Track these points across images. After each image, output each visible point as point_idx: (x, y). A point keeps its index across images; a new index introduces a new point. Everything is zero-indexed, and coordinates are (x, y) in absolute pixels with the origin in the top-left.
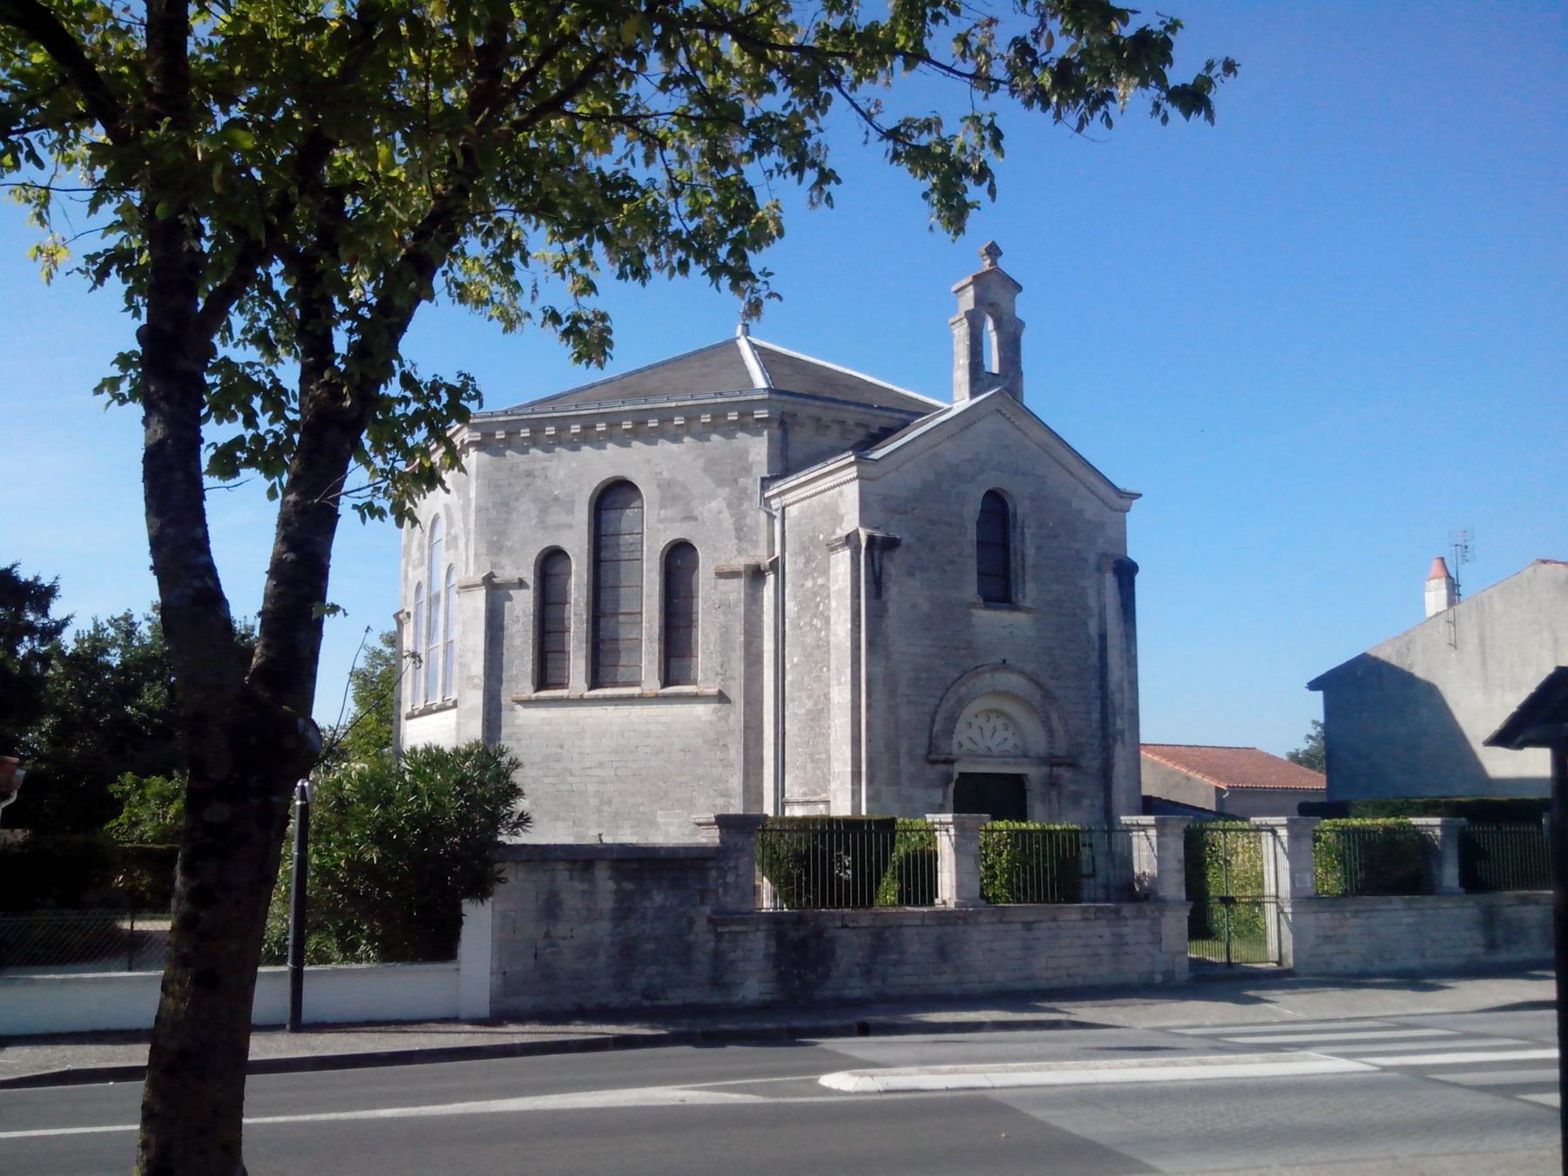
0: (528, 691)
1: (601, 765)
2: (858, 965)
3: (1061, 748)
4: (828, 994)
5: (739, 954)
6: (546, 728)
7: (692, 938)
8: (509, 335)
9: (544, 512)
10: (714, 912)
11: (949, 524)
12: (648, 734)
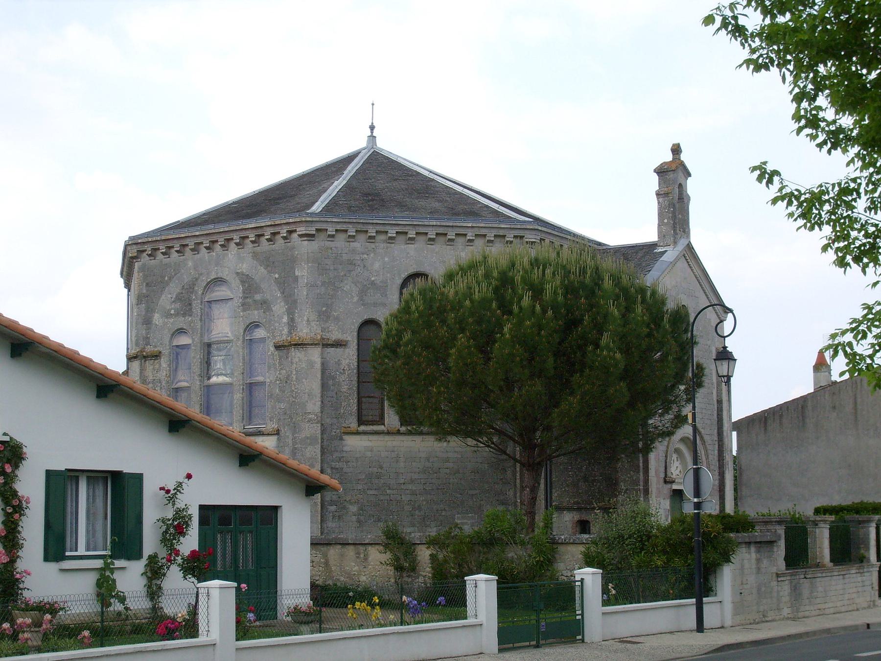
0: (354, 425)
1: (412, 481)
6: (369, 454)
8: (746, 73)
9: (363, 292)
12: (447, 460)
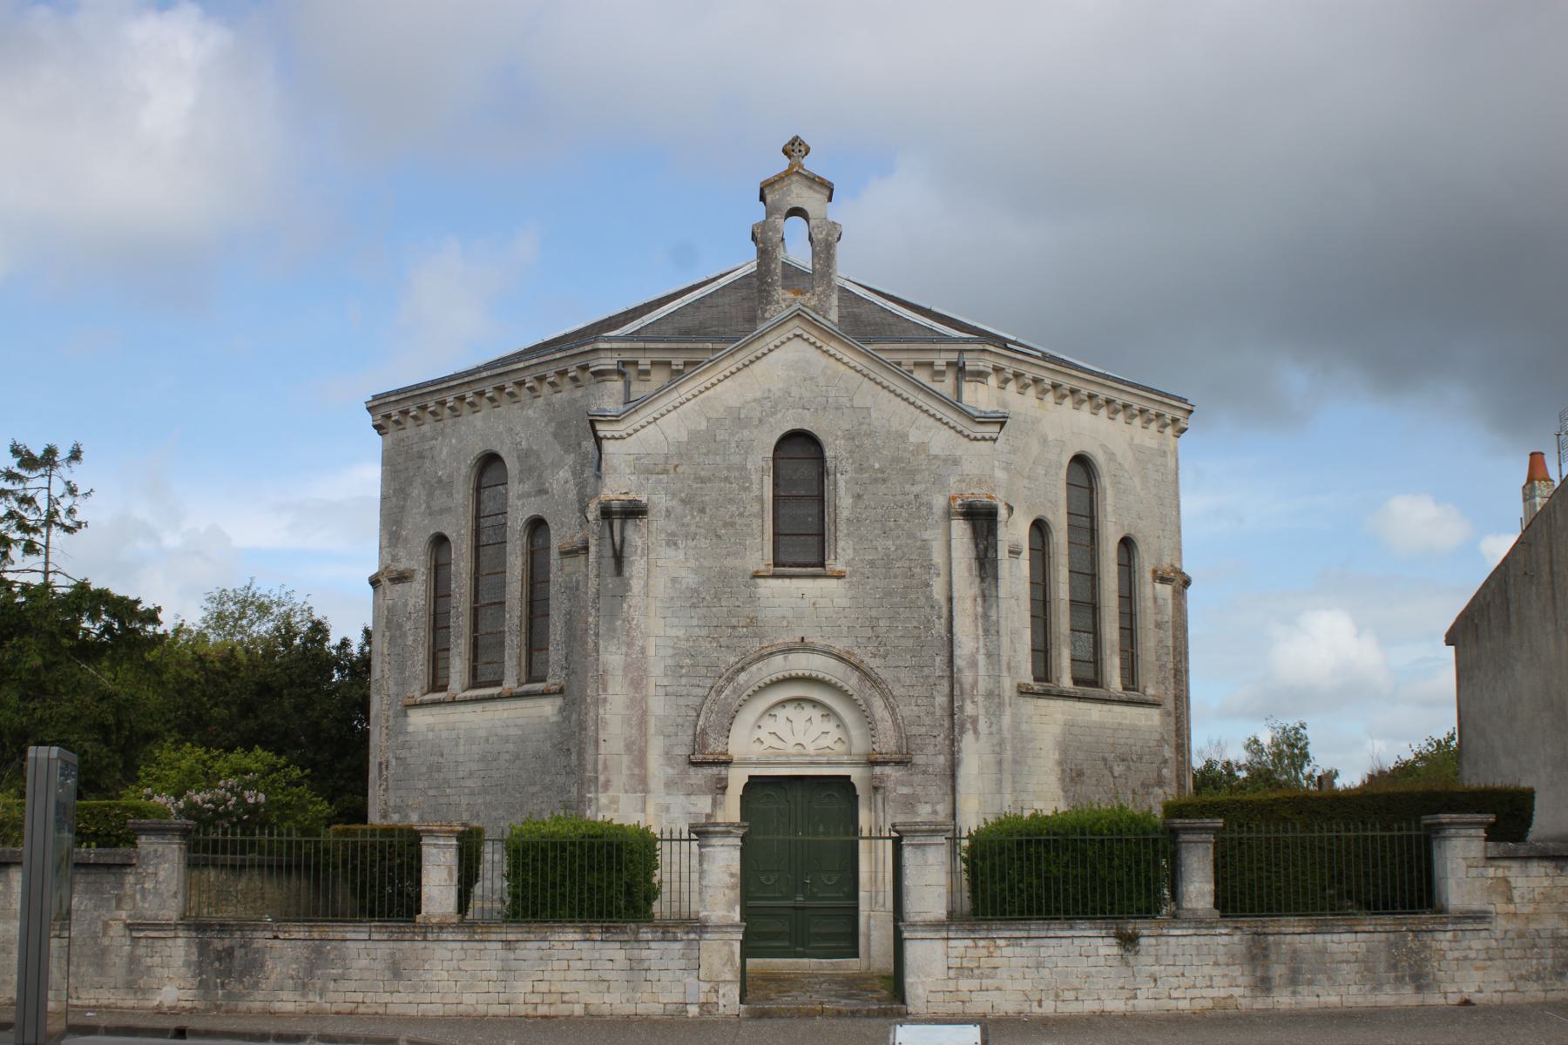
2: (292, 978)
3: (888, 743)
4: (257, 1006)
5: (157, 960)
6: (430, 735)
7: (106, 941)
10: (130, 917)
11: (727, 479)
